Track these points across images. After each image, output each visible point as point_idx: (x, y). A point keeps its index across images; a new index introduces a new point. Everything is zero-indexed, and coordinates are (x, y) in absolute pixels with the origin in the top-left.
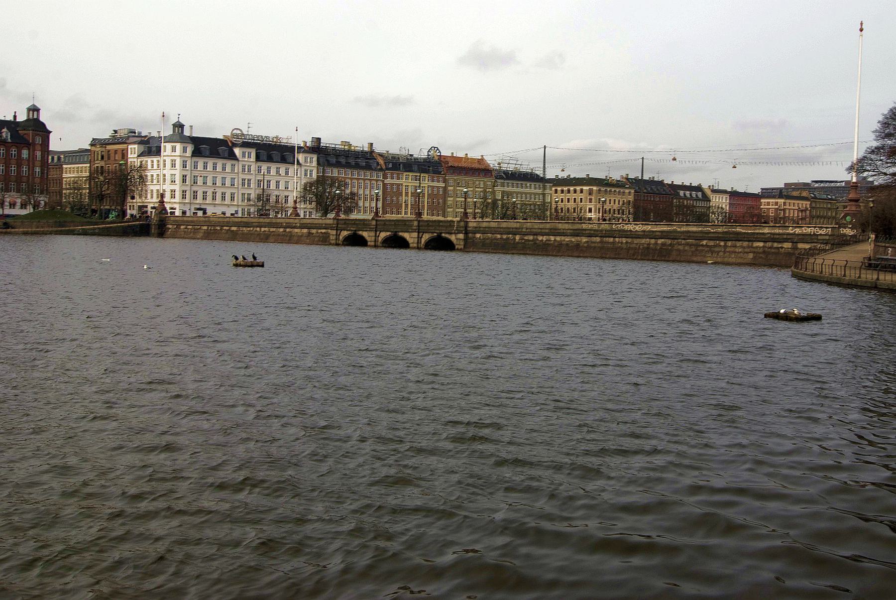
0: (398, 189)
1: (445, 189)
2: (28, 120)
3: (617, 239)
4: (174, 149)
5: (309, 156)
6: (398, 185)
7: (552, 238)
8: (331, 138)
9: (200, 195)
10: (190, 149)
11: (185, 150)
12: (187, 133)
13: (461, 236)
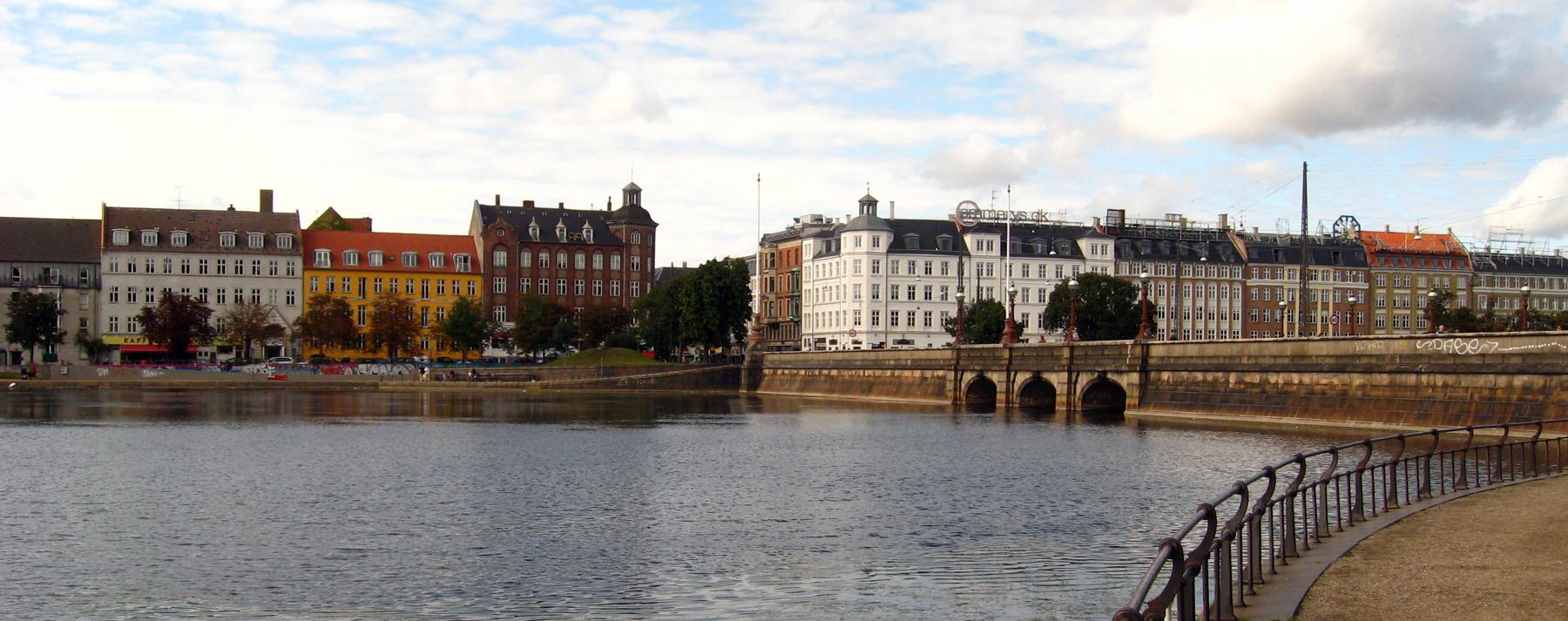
0: (1273, 295)
1: (1369, 294)
2: (624, 208)
3: (1424, 378)
4: (858, 242)
5: (1099, 242)
6: (1273, 289)
7: (1295, 378)
8: (1142, 210)
9: (903, 319)
10: (885, 239)
11: (876, 243)
12: (883, 212)
13: (1135, 378)
